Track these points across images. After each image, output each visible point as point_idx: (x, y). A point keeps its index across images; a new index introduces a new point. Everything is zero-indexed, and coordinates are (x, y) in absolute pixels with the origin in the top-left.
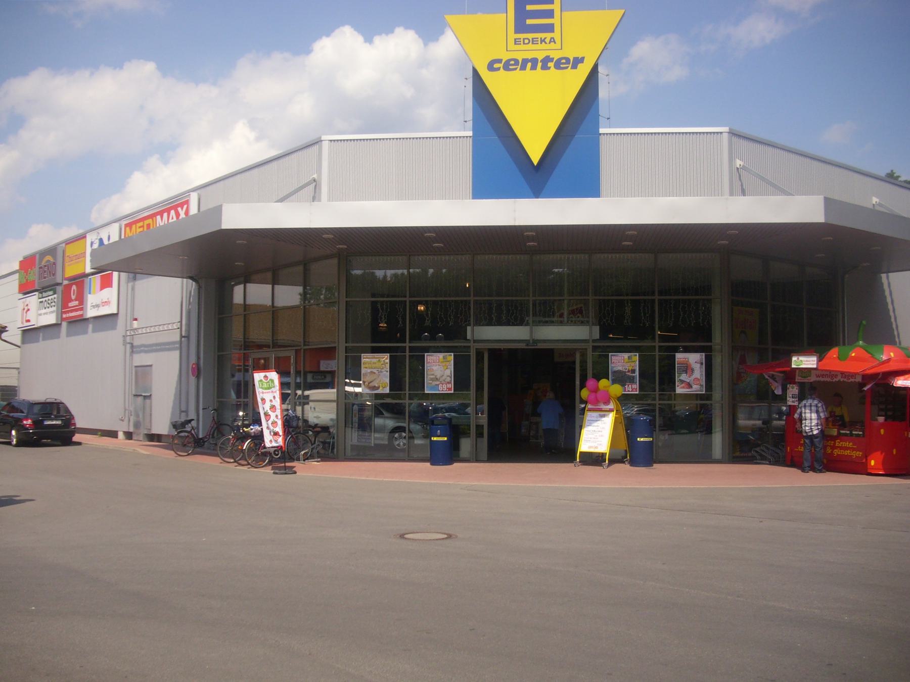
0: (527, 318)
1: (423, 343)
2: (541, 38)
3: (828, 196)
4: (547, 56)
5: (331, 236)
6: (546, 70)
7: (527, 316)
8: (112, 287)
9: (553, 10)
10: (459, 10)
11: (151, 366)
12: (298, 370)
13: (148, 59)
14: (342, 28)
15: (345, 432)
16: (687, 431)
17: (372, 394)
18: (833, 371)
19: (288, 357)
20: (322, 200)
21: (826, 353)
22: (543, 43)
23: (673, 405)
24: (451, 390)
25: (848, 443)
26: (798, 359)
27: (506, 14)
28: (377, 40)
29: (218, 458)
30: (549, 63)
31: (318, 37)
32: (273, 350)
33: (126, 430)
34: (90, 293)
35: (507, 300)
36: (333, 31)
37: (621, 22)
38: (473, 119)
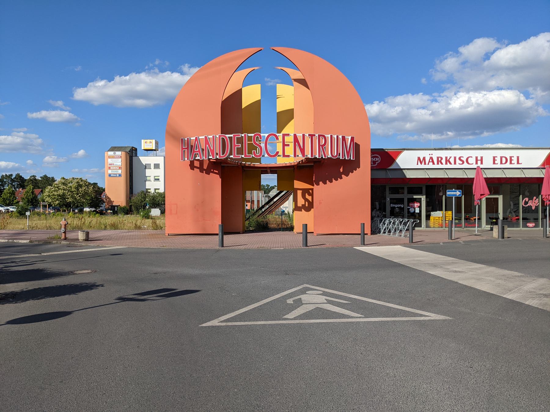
0: (441, 244)
1: (520, 217)
2: (446, 158)
3: (544, 179)
4: (360, 167)
5: (294, 203)
6: (65, 316)
7: (439, 243)
9: (498, 198)
10: (222, 180)
11: (150, 176)
12: (253, 200)
13: (377, 101)
14: (475, 40)
15: (306, 304)
16: (37, 136)
17: (522, 221)
18: (371, 163)
20: (445, 158)
21: (128, 102)
22: (448, 163)
23: (304, 246)
24: (497, 199)
25: (75, 223)
26: (115, 153)
27: (148, 177)
28: (415, 95)
29: (38, 196)
30: (321, 182)
31: (479, 37)
32: (465, 229)
33: (370, 234)
34: (259, 161)
35: (464, 219)
36: (521, 41)
37: (94, 306)
38: (468, 178)
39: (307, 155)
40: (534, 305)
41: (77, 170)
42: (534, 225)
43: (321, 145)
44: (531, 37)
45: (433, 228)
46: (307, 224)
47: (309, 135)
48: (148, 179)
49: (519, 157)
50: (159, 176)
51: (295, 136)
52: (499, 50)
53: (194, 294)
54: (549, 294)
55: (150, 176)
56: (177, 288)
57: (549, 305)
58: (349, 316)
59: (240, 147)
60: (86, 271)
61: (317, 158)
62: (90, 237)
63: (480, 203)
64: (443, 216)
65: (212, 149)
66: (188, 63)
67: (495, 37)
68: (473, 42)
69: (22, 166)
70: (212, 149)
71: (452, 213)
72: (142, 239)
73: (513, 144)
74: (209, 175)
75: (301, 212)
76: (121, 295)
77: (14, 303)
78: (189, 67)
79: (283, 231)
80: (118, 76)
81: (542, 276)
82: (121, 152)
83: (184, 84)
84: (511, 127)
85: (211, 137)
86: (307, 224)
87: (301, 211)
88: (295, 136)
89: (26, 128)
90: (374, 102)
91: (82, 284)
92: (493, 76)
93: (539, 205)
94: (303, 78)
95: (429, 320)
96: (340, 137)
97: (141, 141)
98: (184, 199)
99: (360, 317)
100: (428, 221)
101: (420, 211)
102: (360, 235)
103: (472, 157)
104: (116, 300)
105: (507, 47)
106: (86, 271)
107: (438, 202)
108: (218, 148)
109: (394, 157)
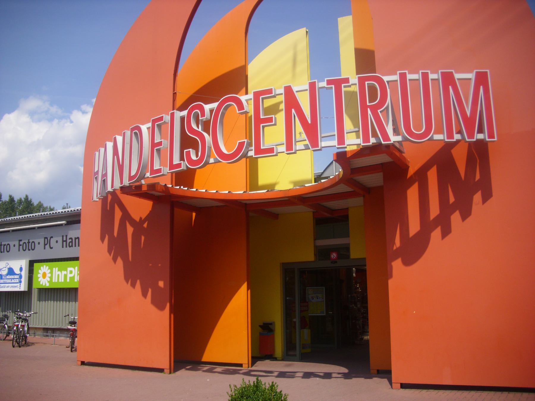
5: (249, 291)
19: (376, 72)
39: (218, 191)
41: (452, 199)
43: (369, 106)
44: (112, 196)
45: (58, 213)
47: (329, 82)
49: (403, 382)
50: (79, 246)
51: (288, 91)
52: (175, 101)
53: (394, 107)
54: (1, 288)
58: (175, 101)
59: (379, 111)
61: (254, 156)
62: (393, 382)
65: (293, 111)
67: (84, 107)
70: (293, 111)
71: (361, 140)
73: (194, 220)
74: (290, 86)
75: (80, 258)
76: (18, 250)
77: (188, 367)
80: (85, 362)
85: (396, 77)
87: (368, 341)
88: (288, 91)
90: (120, 261)
93: (74, 276)
97: (64, 281)
98: (218, 52)
99: (12, 321)
100: (278, 359)
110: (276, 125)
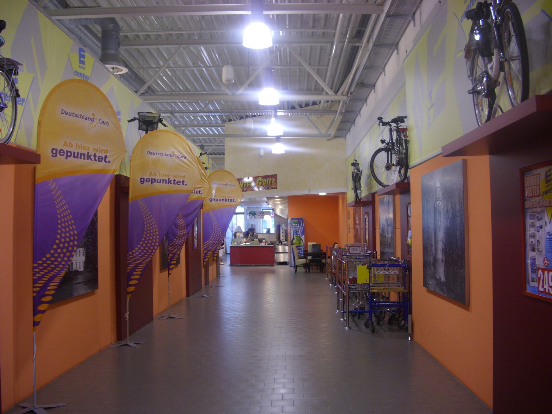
8: (276, 175)
40: (385, 197)
42: (381, 233)
46: (320, 245)
48: (243, 216)
55: (412, 238)
56: (134, 344)
57: (416, 1)
60: (367, 237)
63: (332, 275)
64: (514, 57)
66: (246, 177)
68: (516, 44)
69: (59, 6)
72: (550, 189)
78: (202, 206)
79: (411, 255)
81: (102, 46)
82: (400, 227)
83: (462, 187)
84: (124, 138)
86: (320, 245)
89: (48, 257)
91: (387, 233)
92: (331, 75)
94: (529, 98)
95: (17, 95)
96: (406, 260)
101: (372, 199)
102: (391, 293)
103: (380, 119)
104: (287, 105)
105: (299, 107)
106: (367, 237)
107: (358, 258)
108: (519, 61)
109: (16, 165)
110: (276, 175)
